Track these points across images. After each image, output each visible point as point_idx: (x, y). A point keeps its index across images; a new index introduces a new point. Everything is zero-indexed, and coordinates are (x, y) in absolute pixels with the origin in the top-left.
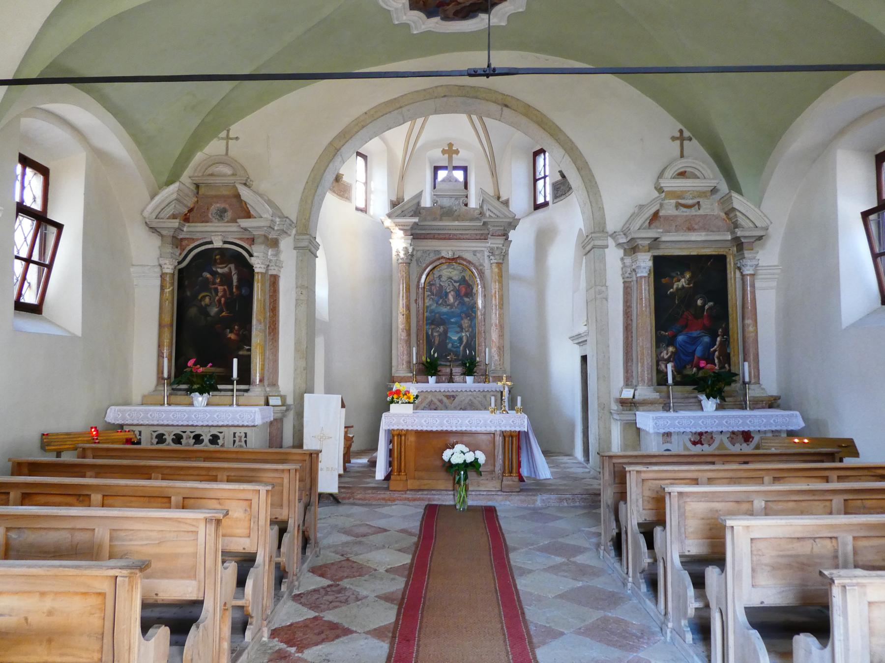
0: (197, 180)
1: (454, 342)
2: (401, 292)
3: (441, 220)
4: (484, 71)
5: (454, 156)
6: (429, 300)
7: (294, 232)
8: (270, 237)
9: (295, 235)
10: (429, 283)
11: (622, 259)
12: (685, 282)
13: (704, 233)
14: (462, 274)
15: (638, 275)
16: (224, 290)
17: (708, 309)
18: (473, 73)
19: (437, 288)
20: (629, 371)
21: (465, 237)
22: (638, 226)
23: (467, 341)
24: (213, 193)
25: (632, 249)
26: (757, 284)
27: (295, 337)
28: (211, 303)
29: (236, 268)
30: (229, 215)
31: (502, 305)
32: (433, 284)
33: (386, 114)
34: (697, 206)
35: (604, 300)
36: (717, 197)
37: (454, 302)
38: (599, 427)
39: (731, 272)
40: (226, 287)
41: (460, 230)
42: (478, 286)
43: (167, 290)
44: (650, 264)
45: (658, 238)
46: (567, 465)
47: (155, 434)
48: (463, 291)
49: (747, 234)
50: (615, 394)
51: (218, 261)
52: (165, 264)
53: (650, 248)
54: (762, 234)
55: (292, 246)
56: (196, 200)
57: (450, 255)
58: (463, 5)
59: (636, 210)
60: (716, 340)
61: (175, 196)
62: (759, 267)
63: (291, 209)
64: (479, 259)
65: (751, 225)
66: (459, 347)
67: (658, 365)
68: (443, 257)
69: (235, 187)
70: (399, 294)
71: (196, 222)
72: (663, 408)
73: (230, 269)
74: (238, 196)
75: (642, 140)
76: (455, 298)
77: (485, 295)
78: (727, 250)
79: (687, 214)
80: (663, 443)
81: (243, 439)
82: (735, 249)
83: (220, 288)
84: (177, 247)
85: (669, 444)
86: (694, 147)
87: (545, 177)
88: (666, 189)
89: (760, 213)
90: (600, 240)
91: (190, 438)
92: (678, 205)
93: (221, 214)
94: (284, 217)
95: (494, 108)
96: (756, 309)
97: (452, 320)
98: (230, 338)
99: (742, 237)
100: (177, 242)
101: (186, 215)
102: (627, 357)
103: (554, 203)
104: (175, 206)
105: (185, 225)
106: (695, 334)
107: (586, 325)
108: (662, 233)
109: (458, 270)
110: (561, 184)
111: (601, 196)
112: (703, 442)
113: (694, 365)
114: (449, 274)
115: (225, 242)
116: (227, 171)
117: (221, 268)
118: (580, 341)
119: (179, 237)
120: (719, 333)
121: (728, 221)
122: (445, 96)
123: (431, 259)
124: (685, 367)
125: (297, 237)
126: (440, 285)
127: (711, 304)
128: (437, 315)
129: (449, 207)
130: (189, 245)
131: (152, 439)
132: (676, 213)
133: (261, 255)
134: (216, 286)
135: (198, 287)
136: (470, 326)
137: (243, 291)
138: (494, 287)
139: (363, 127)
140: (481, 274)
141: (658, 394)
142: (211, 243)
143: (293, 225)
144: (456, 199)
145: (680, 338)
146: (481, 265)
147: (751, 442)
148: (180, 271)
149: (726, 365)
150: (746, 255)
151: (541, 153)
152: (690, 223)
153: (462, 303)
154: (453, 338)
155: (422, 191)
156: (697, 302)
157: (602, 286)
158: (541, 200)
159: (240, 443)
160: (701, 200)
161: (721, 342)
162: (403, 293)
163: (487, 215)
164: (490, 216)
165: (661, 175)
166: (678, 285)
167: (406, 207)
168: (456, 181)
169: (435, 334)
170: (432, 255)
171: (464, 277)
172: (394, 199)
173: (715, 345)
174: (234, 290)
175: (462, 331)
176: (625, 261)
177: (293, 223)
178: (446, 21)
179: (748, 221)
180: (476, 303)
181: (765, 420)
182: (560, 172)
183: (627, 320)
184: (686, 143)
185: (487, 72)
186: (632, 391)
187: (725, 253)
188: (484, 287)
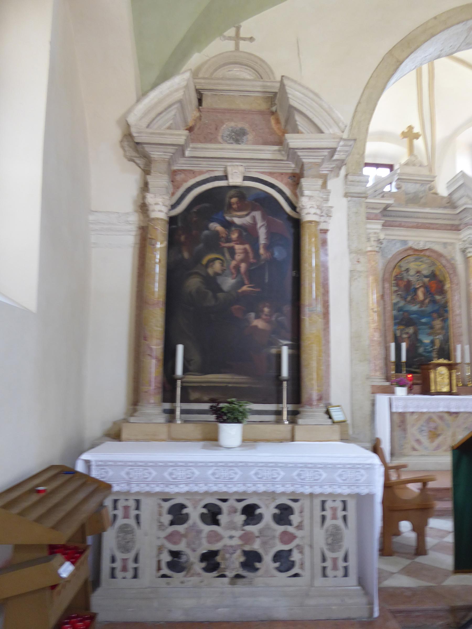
0: (202, 84)
1: (426, 345)
14: (432, 268)
16: (245, 251)
24: (224, 106)
28: (223, 271)
37: (425, 299)
40: (247, 246)
47: (167, 505)
51: (235, 206)
52: (157, 204)
56: (198, 114)
68: (411, 248)
73: (254, 218)
83: (238, 248)
98: (256, 327)
114: (416, 267)
115: (246, 178)
136: (443, 328)
137: (276, 254)
144: (422, 184)
146: (453, 259)
153: (434, 302)
159: (334, 522)
174: (262, 251)
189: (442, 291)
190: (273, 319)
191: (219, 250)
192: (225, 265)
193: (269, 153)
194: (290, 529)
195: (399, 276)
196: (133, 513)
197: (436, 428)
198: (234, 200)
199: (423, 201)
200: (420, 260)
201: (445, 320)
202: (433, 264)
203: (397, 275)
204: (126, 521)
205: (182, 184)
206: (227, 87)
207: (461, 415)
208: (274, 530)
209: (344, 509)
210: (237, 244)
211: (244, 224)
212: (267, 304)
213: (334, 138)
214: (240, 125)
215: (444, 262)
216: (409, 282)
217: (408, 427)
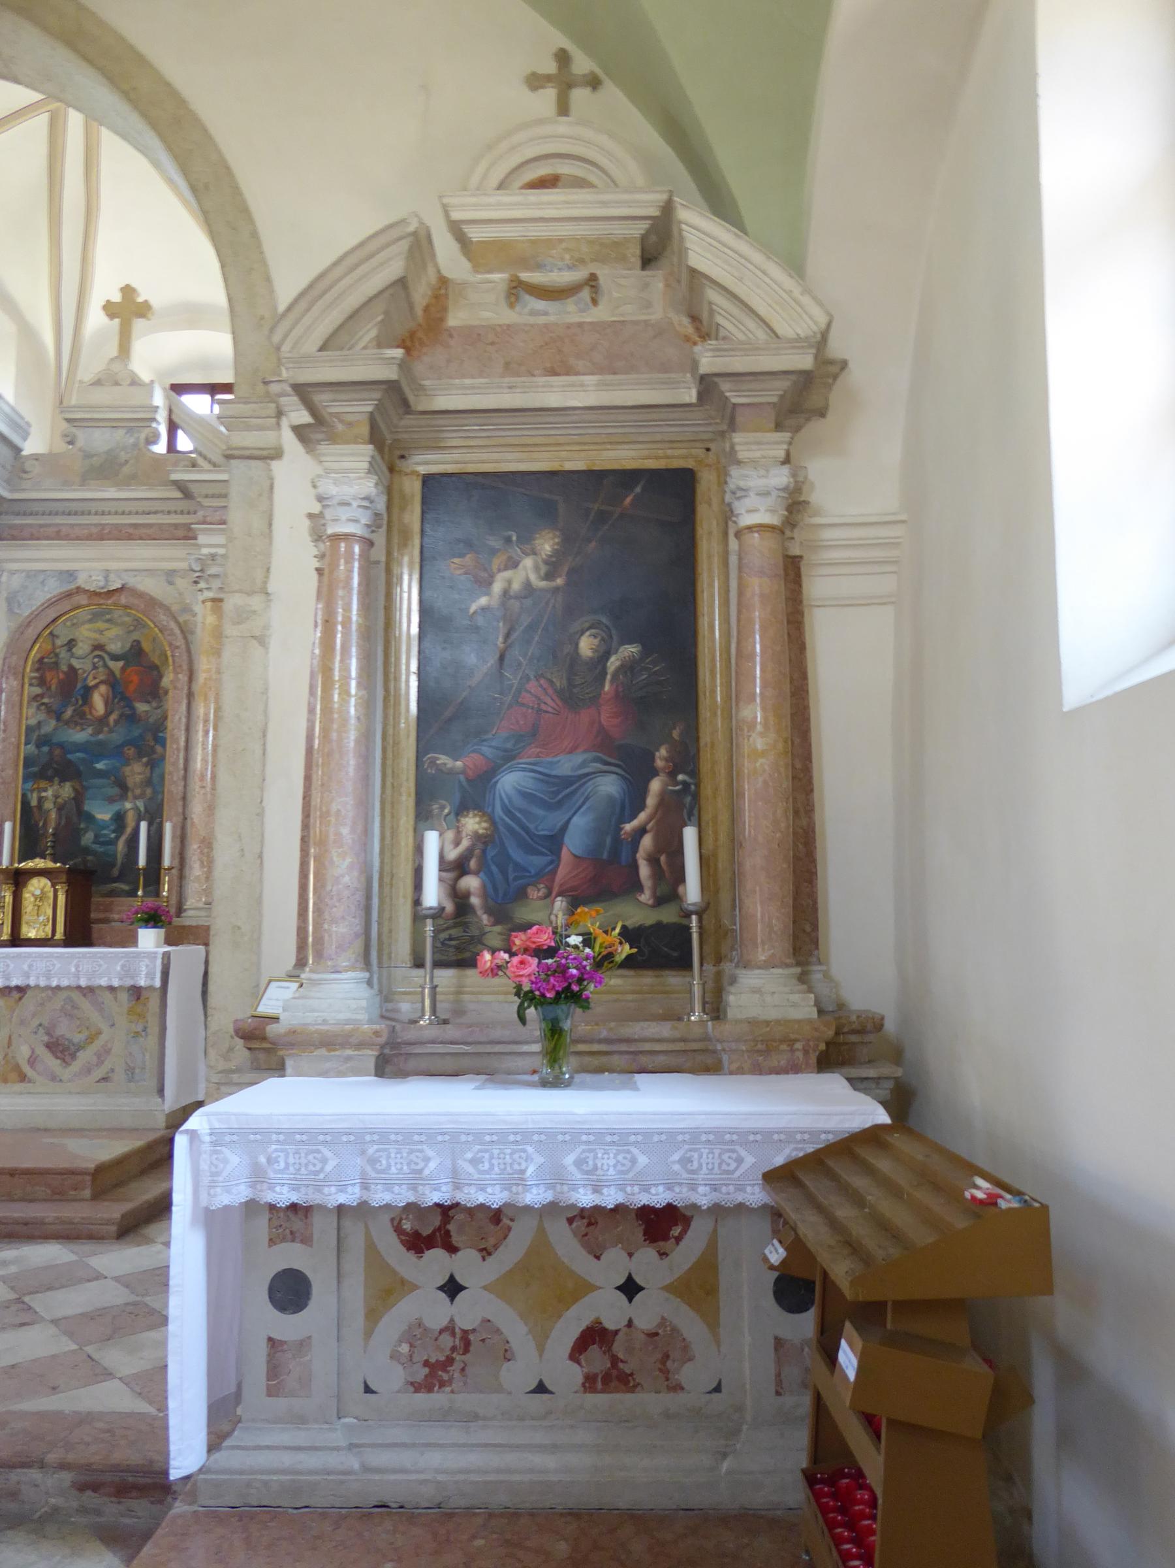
6: (38, 708)
12: (537, 568)
14: (136, 636)
19: (61, 676)
34: (586, 294)
35: (254, 642)
37: (108, 714)
49: (738, 364)
64: (180, 594)
65: (761, 335)
66: (113, 843)
68: (79, 590)
78: (701, 453)
79: (552, 318)
80: (272, 1242)
85: (297, 1247)
92: (517, 290)
97: (100, 766)
106: (566, 765)
111: (268, 279)
112: (456, 1240)
113: (556, 890)
114: (96, 636)
120: (659, 763)
123: (49, 596)
124: (521, 895)
126: (71, 668)
127: (631, 650)
128: (57, 752)
129: (108, 452)
132: (508, 316)
136: (149, 782)
145: (510, 782)
146: (187, 609)
147: (678, 1240)
150: (742, 455)
152: (560, 351)
153: (131, 718)
154: (99, 816)
156: (577, 644)
157: (250, 593)
161: (664, 800)
173: (642, 807)
179: (751, 324)
181: (643, 1160)
187: (689, 464)
189: (154, 691)
193: (353, 459)
195: (46, 660)
199: (126, 470)
200: (104, 618)
201: (155, 763)
202: (138, 624)
206: (739, 396)
207: (29, 993)
215: (163, 618)
216: (72, 670)
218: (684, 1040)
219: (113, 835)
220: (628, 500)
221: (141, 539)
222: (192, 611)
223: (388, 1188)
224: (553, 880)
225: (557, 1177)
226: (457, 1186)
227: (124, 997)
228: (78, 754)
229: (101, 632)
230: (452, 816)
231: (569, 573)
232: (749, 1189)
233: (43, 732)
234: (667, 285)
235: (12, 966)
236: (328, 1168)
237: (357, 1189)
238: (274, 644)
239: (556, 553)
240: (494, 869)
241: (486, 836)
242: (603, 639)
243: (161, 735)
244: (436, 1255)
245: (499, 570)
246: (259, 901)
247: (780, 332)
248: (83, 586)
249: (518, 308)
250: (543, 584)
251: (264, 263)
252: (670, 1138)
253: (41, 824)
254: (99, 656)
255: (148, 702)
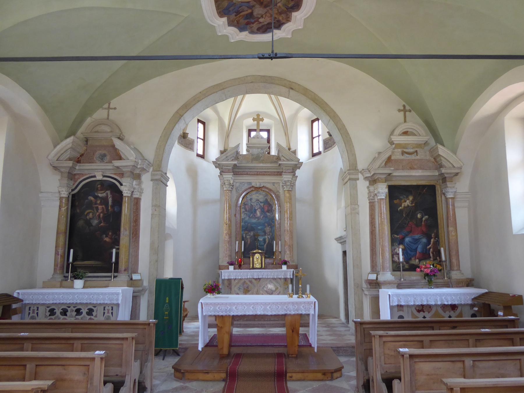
2: (226, 209)
3: (252, 162)
4: (269, 55)
5: (261, 122)
6: (244, 214)
7: (151, 169)
8: (135, 172)
9: (152, 171)
10: (244, 203)
11: (368, 187)
12: (409, 202)
13: (420, 171)
14: (266, 198)
15: (379, 198)
17: (425, 220)
18: (262, 56)
20: (374, 262)
21: (267, 173)
22: (377, 167)
23: (269, 242)
25: (373, 181)
26: (456, 205)
27: (150, 239)
28: (93, 217)
29: (111, 193)
30: (108, 158)
31: (292, 218)
32: (247, 204)
33: (214, 93)
34: (415, 154)
36: (427, 148)
37: (260, 216)
38: (355, 300)
39: (439, 196)
40: (104, 206)
41: (264, 169)
42: (276, 205)
43: (63, 209)
44: (387, 190)
45: (391, 174)
46: (328, 333)
47: (48, 309)
48: (266, 208)
49: (449, 171)
50: (364, 278)
51: (99, 189)
52: (62, 191)
53: (386, 181)
54: (458, 172)
55: (150, 178)
56: (86, 148)
57: (258, 186)
58: (263, 24)
59: (377, 156)
60: (430, 241)
61: (70, 145)
62: (457, 193)
63: (150, 155)
64: (276, 188)
65: (450, 165)
66: (263, 245)
67: (393, 257)
68: (253, 187)
69: (112, 140)
70: (224, 210)
71: (85, 163)
72: (397, 286)
74: (113, 146)
75: (379, 111)
76: (261, 214)
77: (280, 211)
79: (410, 158)
80: (398, 311)
81: (110, 311)
82: (441, 181)
83: (100, 207)
84: (71, 180)
85: (402, 312)
86: (412, 116)
87: (319, 136)
88: (395, 142)
89: (456, 158)
90: (353, 175)
91: (73, 311)
92: (403, 153)
93: (102, 158)
94: (144, 159)
95: (284, 90)
96: (456, 220)
97: (259, 228)
98: (106, 241)
99: (445, 173)
100: (71, 176)
101: (78, 158)
102: (372, 252)
103: (324, 152)
104: (70, 153)
105: (77, 165)
106: (417, 236)
107: (345, 231)
108: (394, 170)
109: (263, 195)
110: (329, 140)
112: (425, 311)
114: (257, 197)
115: (104, 176)
116: (108, 129)
117: (102, 193)
118: (342, 241)
119: (73, 173)
120: (433, 236)
121: (436, 163)
122: (252, 82)
123: (245, 188)
124: (410, 259)
125: (153, 173)
126: (251, 204)
129: (257, 154)
130: (79, 179)
131: (46, 312)
132: (402, 157)
133: (128, 184)
134: (97, 206)
135: (85, 206)
136: (271, 232)
137: (116, 209)
138: (287, 206)
139: (199, 101)
140: (278, 197)
141: (394, 277)
142: (95, 176)
143: (150, 164)
144: (262, 149)
145: (407, 240)
147: (456, 310)
148: (73, 196)
149: (438, 258)
151: (316, 121)
152: (412, 164)
153: (266, 217)
155: (239, 144)
156: (417, 215)
157: (355, 205)
158: (316, 151)
160: (418, 150)
162: (227, 210)
163: (282, 160)
164: (283, 160)
165: (392, 133)
166: (405, 204)
167: (229, 154)
168: (262, 138)
169: (248, 237)
170: (246, 185)
171: (266, 200)
172: (222, 149)
173: (430, 244)
174: (110, 208)
175: (265, 235)
176: (370, 189)
177: (150, 163)
178: (253, 34)
179: (449, 163)
180: (275, 216)
182: (328, 132)
183: (372, 227)
184: (407, 113)
185: (271, 56)
186: (375, 275)
187: (434, 184)
188: (280, 206)
190: (113, 237)
191: (92, 208)
192: (94, 215)
194: (92, 317)
195: (245, 203)
196: (36, 312)
197: (248, 287)
198: (99, 186)
199: (262, 159)
203: (244, 203)
204: (33, 315)
205: (78, 180)
207: (261, 280)
208: (87, 318)
209: (112, 310)
210: (99, 205)
211: (103, 197)
212: (111, 231)
213: (132, 162)
214: (104, 152)
216: (252, 206)
217: (233, 287)
218: (445, 282)
219: (263, 244)
220: (425, 190)
221: (267, 175)
222: (279, 192)
223: (418, 302)
224: (416, 256)
225: (442, 300)
226: (427, 302)
227: (283, 280)
228: (254, 225)
229: (258, 197)
230: (398, 245)
231: (415, 203)
232: (469, 301)
233: (246, 220)
234: (429, 152)
235: (259, 274)
236: (409, 300)
237: (413, 303)
238: (360, 214)
239: (412, 200)
240: (406, 255)
241: (404, 249)
242: (422, 215)
243: (273, 221)
244: (422, 313)
245: (403, 202)
246: (361, 260)
247: (455, 166)
248: (254, 186)
249: (404, 156)
250: (411, 205)
251: (352, 143)
252: (461, 294)
253: (246, 241)
254: (258, 202)
255: (270, 213)
